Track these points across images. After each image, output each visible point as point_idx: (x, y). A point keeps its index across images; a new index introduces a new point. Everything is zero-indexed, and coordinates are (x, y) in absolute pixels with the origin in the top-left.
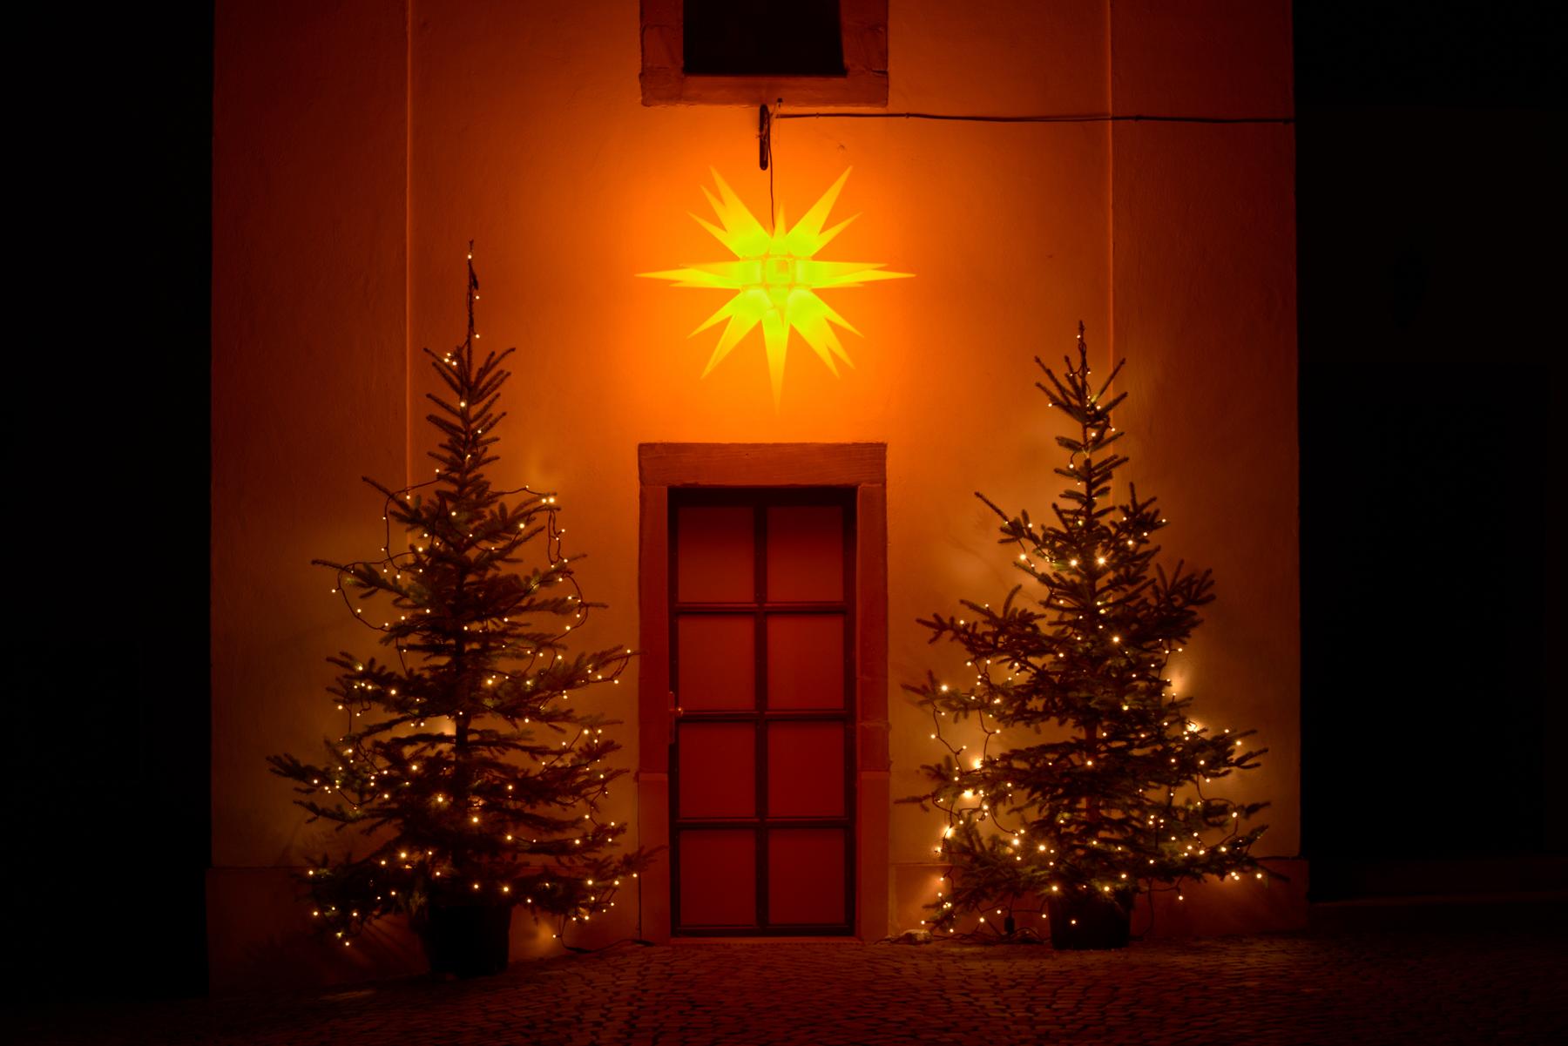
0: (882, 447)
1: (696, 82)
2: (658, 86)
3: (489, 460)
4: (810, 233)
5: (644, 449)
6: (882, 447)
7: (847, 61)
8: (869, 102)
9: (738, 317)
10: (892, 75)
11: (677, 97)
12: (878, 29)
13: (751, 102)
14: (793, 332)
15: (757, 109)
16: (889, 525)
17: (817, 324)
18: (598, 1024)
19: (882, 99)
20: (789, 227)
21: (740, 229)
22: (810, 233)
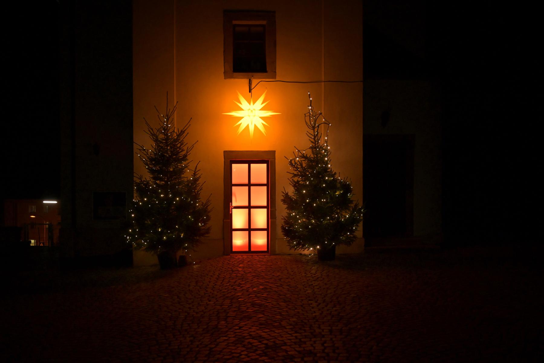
0: (275, 151)
1: (235, 74)
2: (227, 75)
3: (179, 135)
4: (259, 104)
5: (225, 152)
6: (275, 151)
7: (267, 70)
8: (272, 78)
9: (243, 124)
10: (277, 73)
11: (232, 77)
12: (274, 62)
13: (247, 78)
14: (255, 126)
15: (248, 80)
16: (276, 172)
17: (260, 124)
18: (212, 276)
19: (275, 78)
20: (254, 103)
21: (244, 103)
22: (259, 104)
